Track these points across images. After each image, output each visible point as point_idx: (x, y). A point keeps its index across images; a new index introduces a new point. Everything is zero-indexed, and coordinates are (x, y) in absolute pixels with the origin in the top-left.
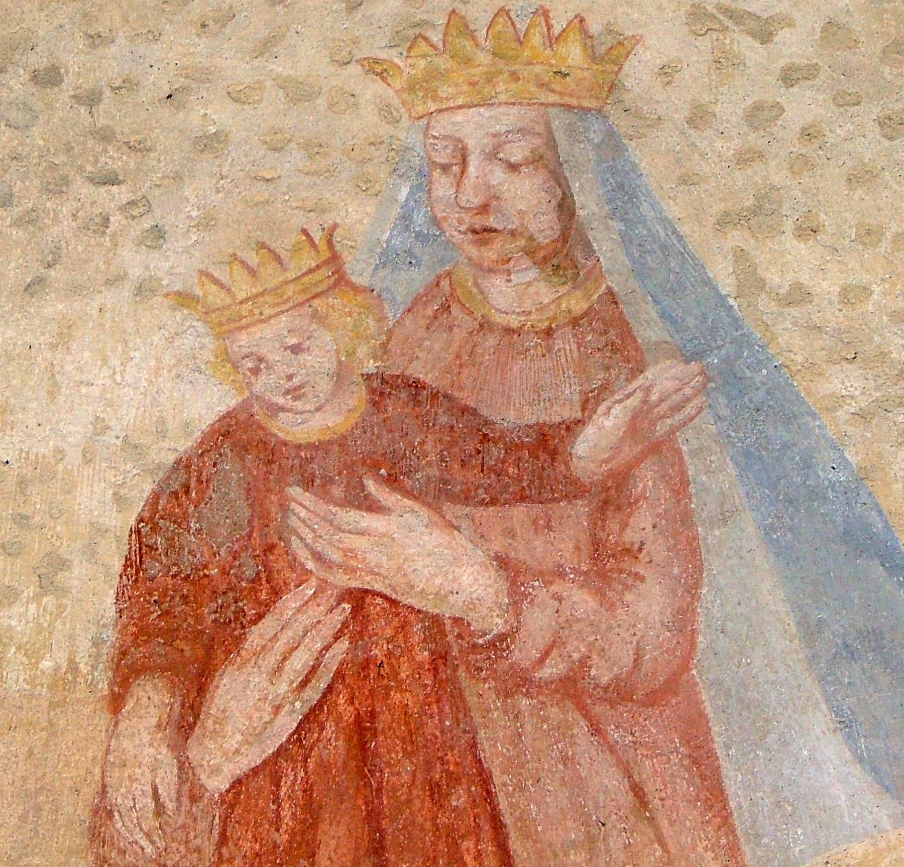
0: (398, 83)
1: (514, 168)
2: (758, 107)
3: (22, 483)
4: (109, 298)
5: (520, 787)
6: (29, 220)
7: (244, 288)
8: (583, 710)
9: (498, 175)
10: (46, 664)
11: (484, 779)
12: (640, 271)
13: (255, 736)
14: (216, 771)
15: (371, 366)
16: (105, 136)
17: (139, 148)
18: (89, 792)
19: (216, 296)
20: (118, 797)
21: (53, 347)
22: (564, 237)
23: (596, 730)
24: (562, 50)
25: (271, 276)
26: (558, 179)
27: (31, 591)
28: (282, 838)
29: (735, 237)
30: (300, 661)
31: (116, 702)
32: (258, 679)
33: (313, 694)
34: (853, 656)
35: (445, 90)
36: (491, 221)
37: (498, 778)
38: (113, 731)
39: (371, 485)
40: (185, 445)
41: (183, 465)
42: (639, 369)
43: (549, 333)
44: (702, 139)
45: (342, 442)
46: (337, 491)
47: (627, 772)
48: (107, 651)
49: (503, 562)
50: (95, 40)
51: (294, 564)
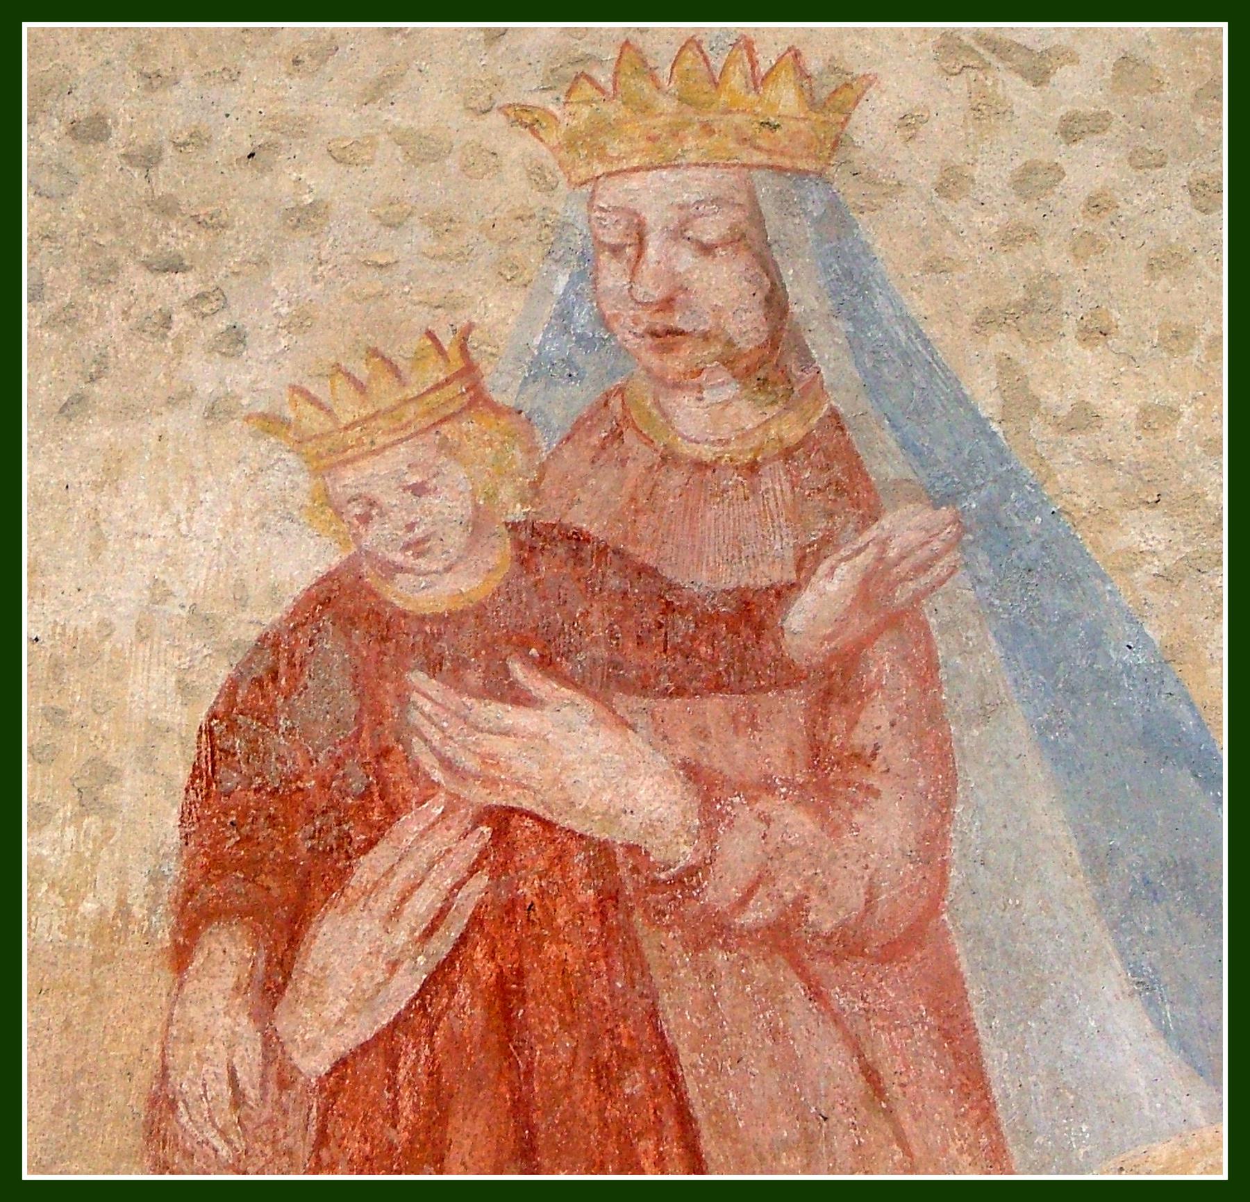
0: (554, 137)
1: (706, 249)
2: (1030, 169)
4: (171, 422)
5: (716, 1069)
7: (349, 409)
9: (686, 259)
10: (89, 906)
11: (668, 1058)
12: (873, 387)
13: (364, 1002)
15: (518, 512)
16: (166, 208)
17: (212, 224)
18: (144, 1076)
19: (313, 420)
20: (183, 1082)
21: (97, 487)
22: (774, 342)
23: (816, 993)
24: (770, 93)
25: (386, 393)
26: (766, 265)
29: (1000, 342)
30: (424, 903)
31: (181, 957)
32: (369, 927)
33: (441, 946)
35: (615, 147)
36: (677, 321)
37: (686, 1057)
39: (518, 670)
40: (272, 616)
41: (269, 642)
42: (871, 517)
45: (479, 612)
46: (473, 678)
47: (856, 1048)
49: (692, 772)
51: (416, 773)
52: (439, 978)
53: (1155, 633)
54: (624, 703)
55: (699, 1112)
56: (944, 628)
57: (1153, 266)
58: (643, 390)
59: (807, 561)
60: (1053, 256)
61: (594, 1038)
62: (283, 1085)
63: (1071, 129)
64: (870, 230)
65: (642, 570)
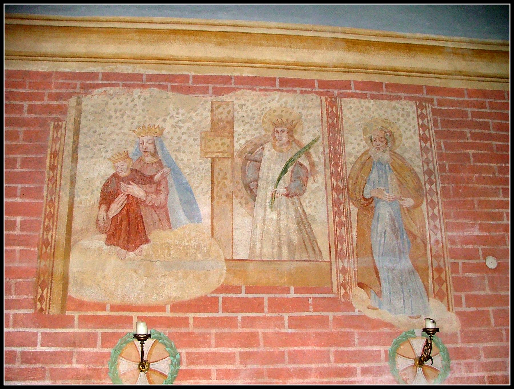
0: (136, 133)
1: (149, 144)
2: (179, 137)
3: (89, 181)
4: (100, 159)
5: (146, 218)
6: (92, 149)
7: (117, 158)
8: (154, 209)
9: (148, 145)
10: (91, 203)
11: (142, 217)
12: (164, 156)
13: (115, 212)
14: (111, 216)
15: (131, 168)
16: (101, 139)
17: (105, 141)
18: (96, 218)
19: (113, 159)
20: (99, 219)
21: (94, 165)
22: (155, 152)
23: (155, 211)
24: (156, 130)
25: (120, 156)
26: (155, 145)
27: (90, 194)
28: (118, 224)
29: (175, 153)
30: (121, 203)
31: (99, 207)
32: (116, 205)
33: (122, 207)
34: (186, 203)
35: (142, 134)
36: (146, 150)
37: (143, 217)
38: (99, 211)
39: (130, 182)
40: (109, 177)
41: (108, 179)
42: (163, 168)
43: (152, 164)
44: (172, 141)
45: (127, 177)
46: (126, 183)
47: (158, 216)
48: (99, 201)
49: (145, 191)
50: (101, 127)
51: (121, 191)
52: (122, 209)
53: (187, 180)
54: (139, 185)
55: (144, 222)
56: (169, 179)
57: (189, 146)
58: (143, 156)
59: (157, 173)
60: (180, 145)
61: (135, 215)
62: (108, 219)
63: (183, 134)
64: (164, 142)
65: (142, 173)
